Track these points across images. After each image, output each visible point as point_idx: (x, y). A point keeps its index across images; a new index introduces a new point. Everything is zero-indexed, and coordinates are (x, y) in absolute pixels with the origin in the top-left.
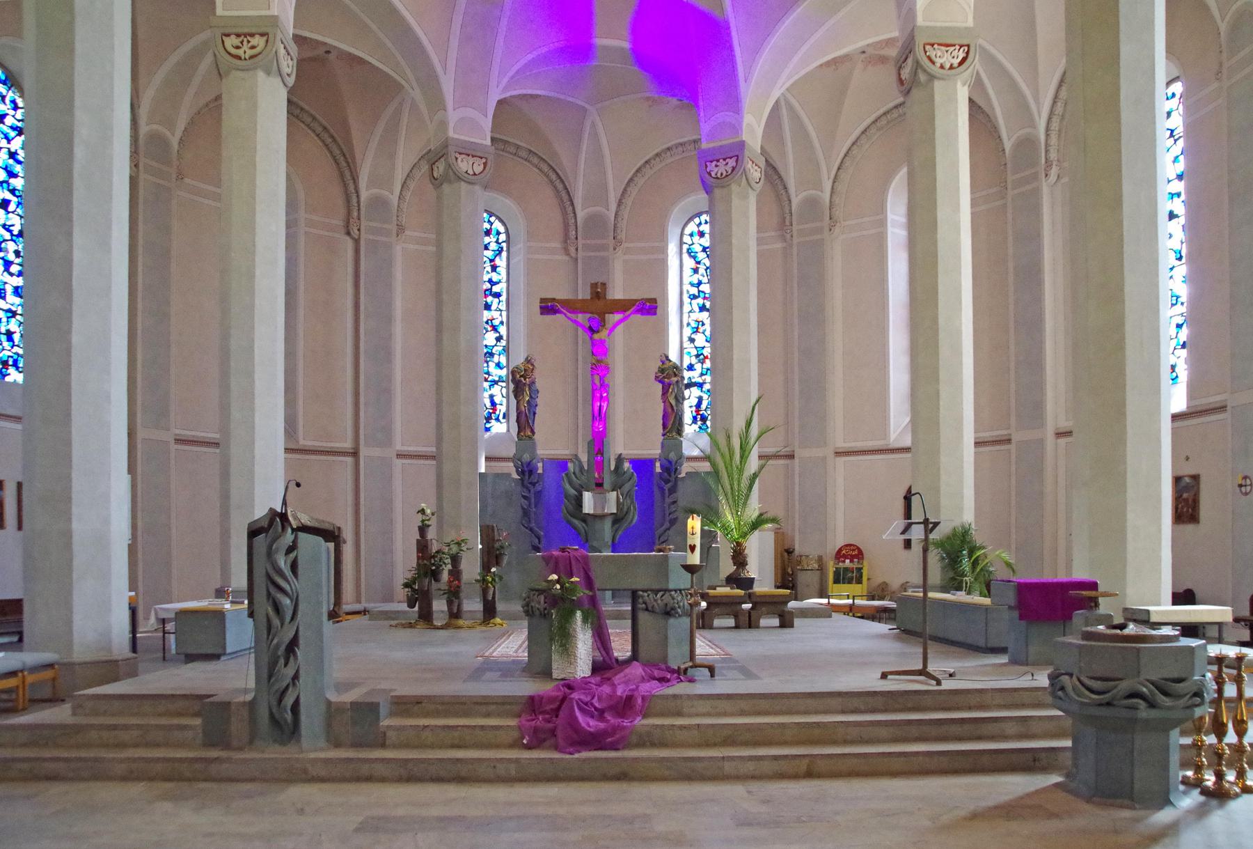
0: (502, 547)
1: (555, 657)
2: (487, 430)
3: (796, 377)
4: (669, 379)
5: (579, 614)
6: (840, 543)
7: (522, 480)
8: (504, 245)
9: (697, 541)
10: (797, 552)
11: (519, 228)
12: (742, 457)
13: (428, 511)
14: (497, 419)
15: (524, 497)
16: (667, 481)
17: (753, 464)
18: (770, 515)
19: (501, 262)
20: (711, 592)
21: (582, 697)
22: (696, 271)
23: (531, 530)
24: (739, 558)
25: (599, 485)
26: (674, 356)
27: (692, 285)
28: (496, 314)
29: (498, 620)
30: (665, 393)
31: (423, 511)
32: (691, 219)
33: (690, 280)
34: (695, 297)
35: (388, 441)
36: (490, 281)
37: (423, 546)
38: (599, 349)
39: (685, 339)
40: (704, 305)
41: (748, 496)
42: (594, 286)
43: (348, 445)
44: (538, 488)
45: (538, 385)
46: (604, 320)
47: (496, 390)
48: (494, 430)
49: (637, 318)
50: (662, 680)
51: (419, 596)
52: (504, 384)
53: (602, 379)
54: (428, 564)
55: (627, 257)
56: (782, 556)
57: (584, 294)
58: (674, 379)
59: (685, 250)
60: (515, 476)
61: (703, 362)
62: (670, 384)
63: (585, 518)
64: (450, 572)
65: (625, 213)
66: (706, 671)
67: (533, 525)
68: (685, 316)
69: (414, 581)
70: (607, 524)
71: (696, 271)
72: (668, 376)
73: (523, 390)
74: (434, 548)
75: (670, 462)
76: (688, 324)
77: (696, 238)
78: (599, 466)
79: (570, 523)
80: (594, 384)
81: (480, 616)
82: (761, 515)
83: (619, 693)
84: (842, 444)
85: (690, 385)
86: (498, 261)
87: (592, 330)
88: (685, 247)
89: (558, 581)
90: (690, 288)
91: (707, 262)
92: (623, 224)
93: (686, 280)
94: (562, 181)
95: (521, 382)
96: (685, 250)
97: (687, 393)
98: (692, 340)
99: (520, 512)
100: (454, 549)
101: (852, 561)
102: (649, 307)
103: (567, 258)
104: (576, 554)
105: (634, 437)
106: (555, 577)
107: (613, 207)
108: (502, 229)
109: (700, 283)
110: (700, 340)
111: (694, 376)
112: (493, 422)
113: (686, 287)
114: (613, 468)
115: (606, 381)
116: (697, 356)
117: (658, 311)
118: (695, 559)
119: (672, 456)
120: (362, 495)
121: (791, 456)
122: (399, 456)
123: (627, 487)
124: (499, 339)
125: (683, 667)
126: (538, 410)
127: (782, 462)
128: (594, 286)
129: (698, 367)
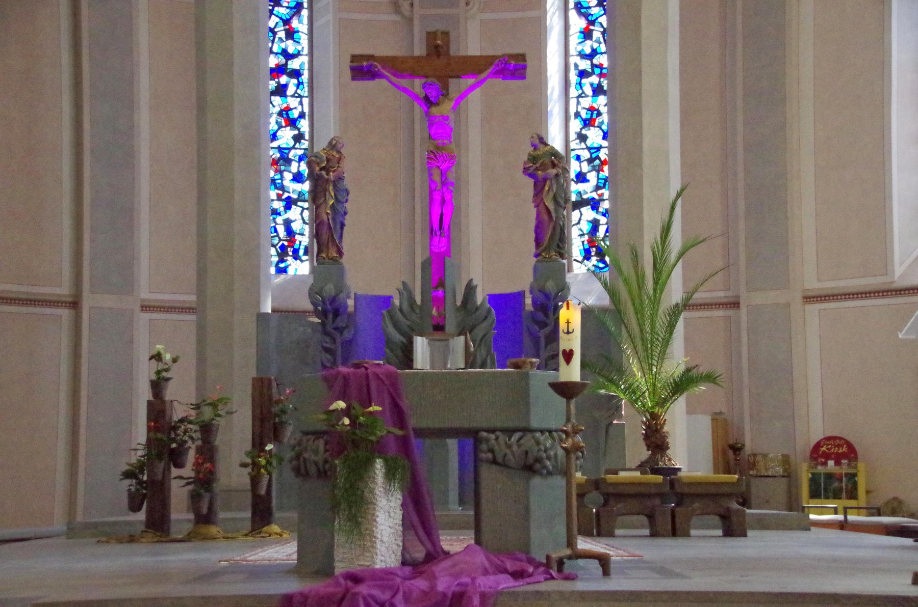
0: (284, 412)
1: (339, 539)
2: (284, 271)
3: (741, 185)
4: (544, 169)
5: (379, 464)
6: (817, 435)
7: (323, 324)
9: (573, 342)
10: (748, 449)
12: (656, 282)
13: (168, 357)
14: (296, 257)
15: (327, 350)
16: (543, 325)
17: (675, 292)
18: (703, 369)
19: (301, 25)
20: (611, 478)
21: (376, 592)
24: (656, 440)
25: (439, 327)
26: (556, 141)
27: (583, 56)
29: (275, 528)
31: (158, 357)
33: (580, 48)
34: (582, 74)
35: (128, 285)
37: (157, 411)
38: (439, 130)
39: (573, 136)
40: (600, 86)
41: (667, 342)
42: (431, 36)
43: (64, 290)
44: (347, 335)
45: (348, 183)
46: (446, 86)
47: (294, 213)
48: (291, 271)
50: (519, 575)
51: (147, 493)
52: (306, 205)
53: (443, 174)
54: (165, 440)
55: (487, 16)
56: (724, 453)
57: (419, 50)
58: (553, 172)
61: (599, 170)
62: (545, 180)
64: (199, 450)
66: (595, 564)
68: (573, 103)
69: (141, 467)
71: (587, 34)
72: (543, 167)
73: (325, 190)
74: (178, 413)
75: (547, 296)
76: (577, 115)
78: (439, 301)
80: (432, 182)
81: (248, 525)
82: (688, 370)
83: (441, 587)
84: (814, 285)
85: (579, 204)
86: (295, 24)
87: (428, 102)
89: (347, 412)
90: (577, 60)
91: (603, 20)
93: (574, 48)
95: (326, 179)
97: (575, 215)
98: (582, 138)
100: (208, 413)
101: (838, 463)
102: (514, 67)
103: (396, 18)
104: (377, 370)
105: (492, 260)
106: (341, 404)
109: (594, 53)
110: (595, 136)
111: (587, 189)
112: (290, 259)
113: (574, 59)
114: (459, 303)
116: (590, 161)
117: (529, 71)
118: (572, 372)
119: (550, 286)
120: (84, 359)
121: (735, 304)
122: (146, 308)
123: (479, 332)
124: (298, 138)
125: (554, 556)
126: (348, 220)
127: (720, 313)
129: (592, 177)
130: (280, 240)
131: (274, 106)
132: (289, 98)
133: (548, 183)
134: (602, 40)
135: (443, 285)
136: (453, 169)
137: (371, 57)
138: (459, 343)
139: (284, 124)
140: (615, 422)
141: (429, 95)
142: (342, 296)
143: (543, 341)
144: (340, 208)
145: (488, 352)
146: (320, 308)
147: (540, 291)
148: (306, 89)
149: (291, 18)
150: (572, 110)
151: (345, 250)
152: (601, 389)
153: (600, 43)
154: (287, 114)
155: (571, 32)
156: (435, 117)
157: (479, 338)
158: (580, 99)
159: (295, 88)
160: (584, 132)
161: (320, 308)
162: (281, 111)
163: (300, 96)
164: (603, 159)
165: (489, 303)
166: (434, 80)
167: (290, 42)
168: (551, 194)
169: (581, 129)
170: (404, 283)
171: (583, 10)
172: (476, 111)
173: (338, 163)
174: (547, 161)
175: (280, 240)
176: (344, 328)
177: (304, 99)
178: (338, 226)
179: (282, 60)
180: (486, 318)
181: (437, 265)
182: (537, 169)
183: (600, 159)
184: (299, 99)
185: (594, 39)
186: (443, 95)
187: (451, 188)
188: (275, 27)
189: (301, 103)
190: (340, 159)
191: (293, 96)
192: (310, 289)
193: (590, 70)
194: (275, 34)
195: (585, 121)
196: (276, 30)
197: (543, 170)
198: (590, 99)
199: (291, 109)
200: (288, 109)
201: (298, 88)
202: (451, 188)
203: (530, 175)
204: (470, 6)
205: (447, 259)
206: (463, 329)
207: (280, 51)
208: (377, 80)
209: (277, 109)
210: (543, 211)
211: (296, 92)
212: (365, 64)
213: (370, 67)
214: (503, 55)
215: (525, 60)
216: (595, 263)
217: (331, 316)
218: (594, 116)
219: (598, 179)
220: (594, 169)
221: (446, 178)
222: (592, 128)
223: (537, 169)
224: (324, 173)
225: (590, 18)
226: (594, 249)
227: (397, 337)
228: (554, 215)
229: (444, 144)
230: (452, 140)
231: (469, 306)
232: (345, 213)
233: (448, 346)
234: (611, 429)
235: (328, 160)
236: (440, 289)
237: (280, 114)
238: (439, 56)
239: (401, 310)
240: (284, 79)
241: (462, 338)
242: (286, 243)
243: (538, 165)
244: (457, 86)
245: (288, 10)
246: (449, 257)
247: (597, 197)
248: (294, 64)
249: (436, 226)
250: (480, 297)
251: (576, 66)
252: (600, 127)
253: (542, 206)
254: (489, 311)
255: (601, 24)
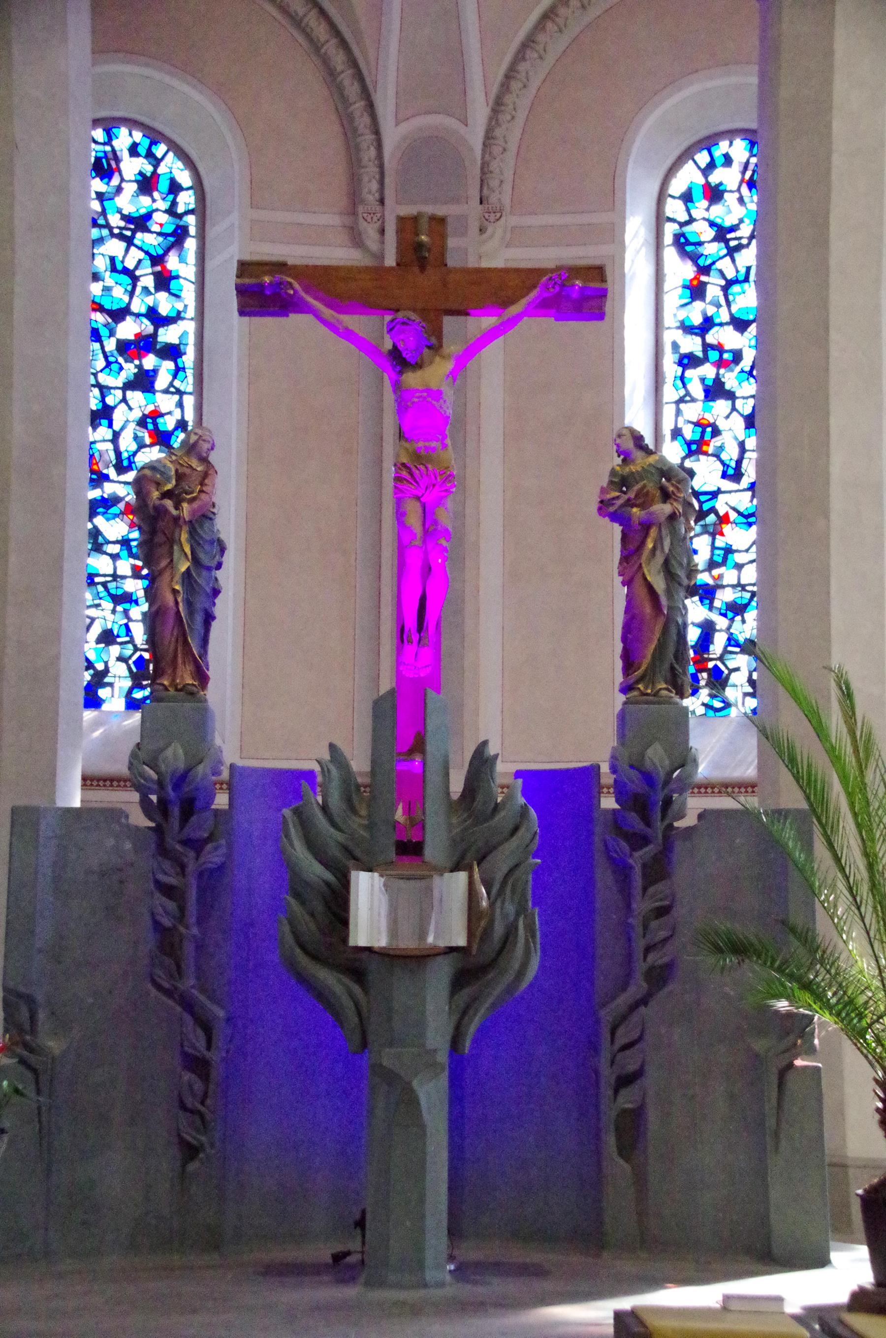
4: (645, 505)
7: (159, 831)
8: (191, 220)
11: (229, 175)
15: (167, 891)
16: (639, 841)
19: (185, 265)
22: (696, 291)
23: (188, 1005)
25: (410, 849)
27: (688, 329)
28: (166, 403)
30: (631, 554)
32: (687, 155)
33: (682, 314)
34: (688, 361)
36: (152, 314)
38: (422, 420)
40: (718, 382)
44: (213, 856)
49: (536, 328)
53: (428, 516)
58: (666, 509)
59: (668, 239)
60: (140, 820)
62: (646, 526)
63: (359, 965)
65: (512, 133)
67: (188, 983)
68: (669, 412)
70: (434, 996)
71: (696, 291)
73: (171, 541)
75: (648, 778)
76: (677, 433)
77: (700, 206)
78: (411, 787)
79: (305, 981)
86: (172, 263)
87: (399, 362)
88: (670, 229)
90: (678, 335)
92: (505, 167)
93: (672, 314)
94: (343, 44)
95: (170, 520)
96: (668, 239)
99: (149, 942)
102: (581, 296)
105: (531, 698)
107: (480, 113)
108: (185, 178)
109: (708, 323)
113: (671, 335)
114: (457, 786)
115: (444, 517)
119: (656, 757)
128: (408, 225)
130: (136, 649)
131: (130, 409)
132: (157, 394)
133: (653, 532)
134: (722, 301)
135: (419, 746)
136: (450, 501)
137: (281, 267)
138: (457, 883)
139: (148, 441)
140: (799, 1062)
141: (402, 345)
142: (201, 770)
143: (638, 880)
144: (201, 580)
145: (521, 910)
146: (154, 798)
147: (632, 767)
148: (190, 379)
149: (167, 251)
150: (667, 426)
151: (212, 673)
152: (778, 997)
153: (719, 306)
154: (155, 425)
155: (667, 286)
156: (412, 392)
157: (499, 876)
158: (682, 406)
159: (170, 378)
160: (688, 464)
161: (154, 798)
162: (145, 417)
163: (179, 392)
164: (721, 513)
165: (524, 794)
166: (414, 316)
167: (162, 296)
168: (660, 559)
169: (683, 459)
170: (332, 747)
171: (689, 248)
172: (496, 382)
173: (202, 484)
174: (651, 487)
175: (136, 649)
176: (207, 841)
177: (185, 397)
178: (199, 618)
179: (147, 327)
180: (516, 829)
181: (406, 713)
182: (629, 503)
183: (717, 514)
184: (176, 397)
185: (708, 298)
186: (430, 347)
187: (443, 541)
188: (137, 267)
189: (180, 405)
190: (206, 475)
191: (166, 391)
192: (134, 755)
193: (700, 354)
194: (135, 279)
195: (689, 444)
196: (138, 273)
197: (642, 506)
198: (699, 405)
199: (162, 415)
200: (156, 415)
201: (175, 376)
202: (443, 541)
203: (615, 517)
204: (485, 236)
205: (430, 693)
206: (463, 857)
207: (143, 310)
208: (293, 317)
209: (137, 414)
210: (641, 592)
211: (171, 384)
212: (267, 279)
213: (278, 286)
214: (558, 268)
215: (603, 280)
216: (707, 700)
217: (176, 811)
218: (707, 436)
219: (713, 547)
220: (705, 530)
221: (436, 522)
222: (702, 457)
223: (629, 503)
224: (169, 503)
225: (701, 262)
226: (705, 675)
227: (315, 871)
228: (664, 601)
229: (434, 449)
230: (448, 441)
231: (478, 804)
232: (216, 592)
233: (429, 890)
234: (790, 1076)
235: (180, 477)
236: (418, 758)
237: (142, 423)
238: (423, 268)
239: (324, 808)
240: (150, 361)
241: (462, 877)
242: (146, 656)
243: (632, 494)
244: (459, 331)
245: (161, 239)
246: (438, 691)
247: (711, 582)
248: (168, 335)
249: (411, 622)
250: (504, 769)
251: (675, 346)
252: (717, 456)
253: (638, 583)
254: (524, 813)
255: (721, 272)
